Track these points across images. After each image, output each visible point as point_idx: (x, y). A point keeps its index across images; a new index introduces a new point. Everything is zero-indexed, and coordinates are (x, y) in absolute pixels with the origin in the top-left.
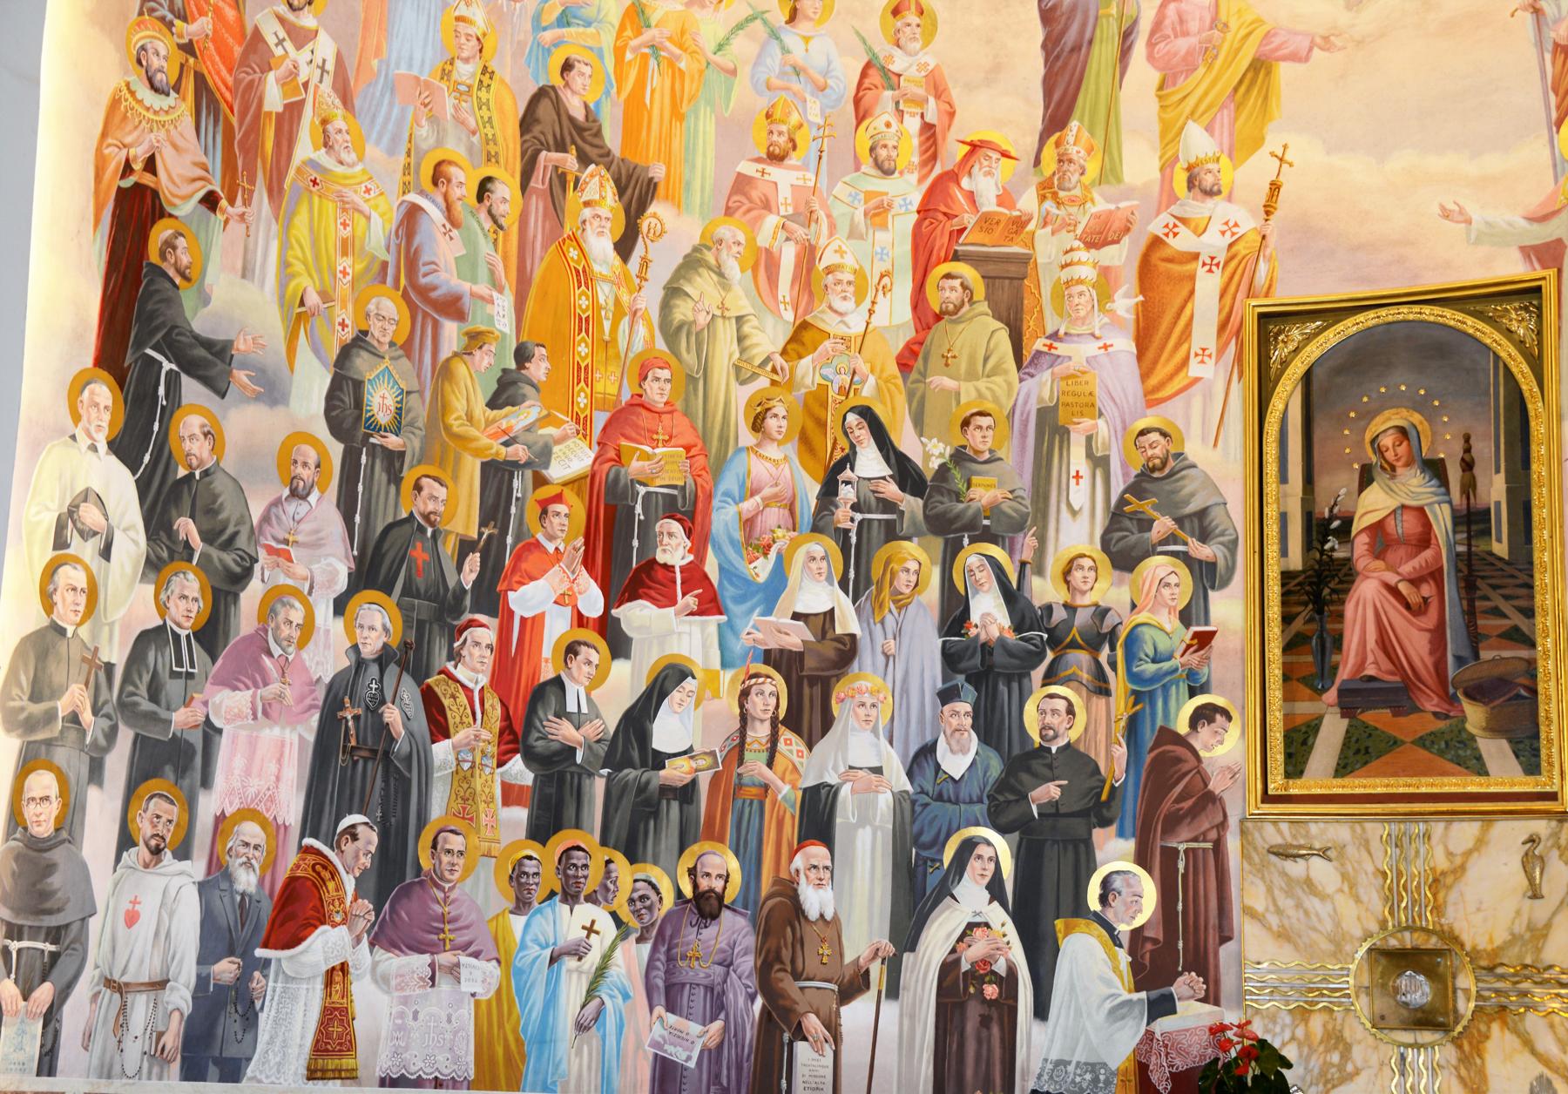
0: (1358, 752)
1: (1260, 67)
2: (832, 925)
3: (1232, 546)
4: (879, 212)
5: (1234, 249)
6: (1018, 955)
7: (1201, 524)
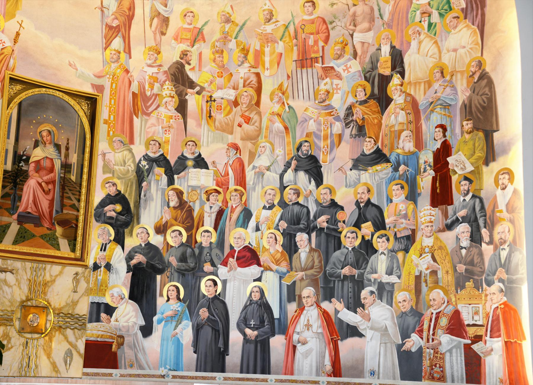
0: (21, 237)
5: (3, 51)
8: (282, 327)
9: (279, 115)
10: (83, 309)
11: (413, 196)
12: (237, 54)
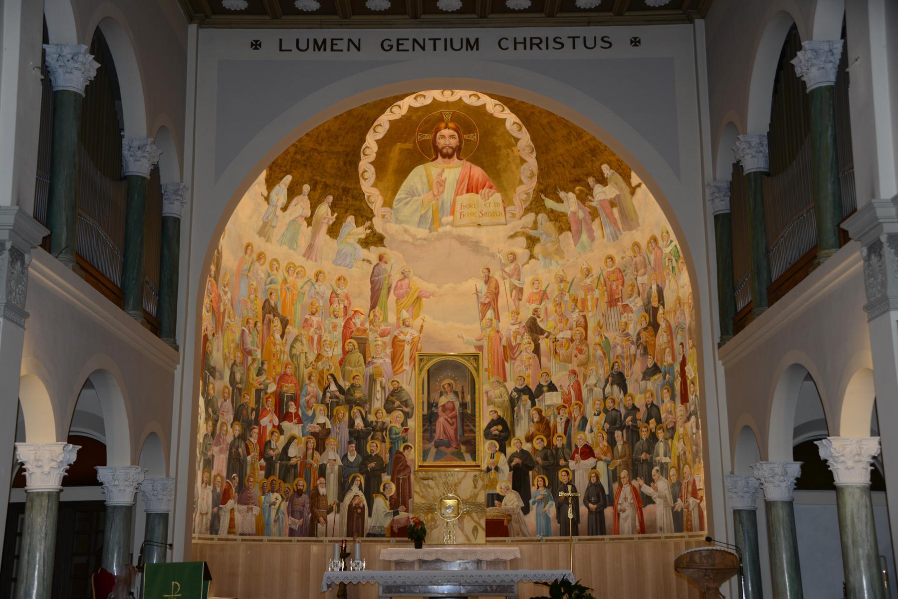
1: (419, 298)
2: (325, 497)
3: (413, 409)
4: (335, 327)
6: (365, 503)
7: (406, 403)
8: (610, 500)
9: (599, 345)
10: (482, 498)
11: (673, 398)
12: (571, 304)
